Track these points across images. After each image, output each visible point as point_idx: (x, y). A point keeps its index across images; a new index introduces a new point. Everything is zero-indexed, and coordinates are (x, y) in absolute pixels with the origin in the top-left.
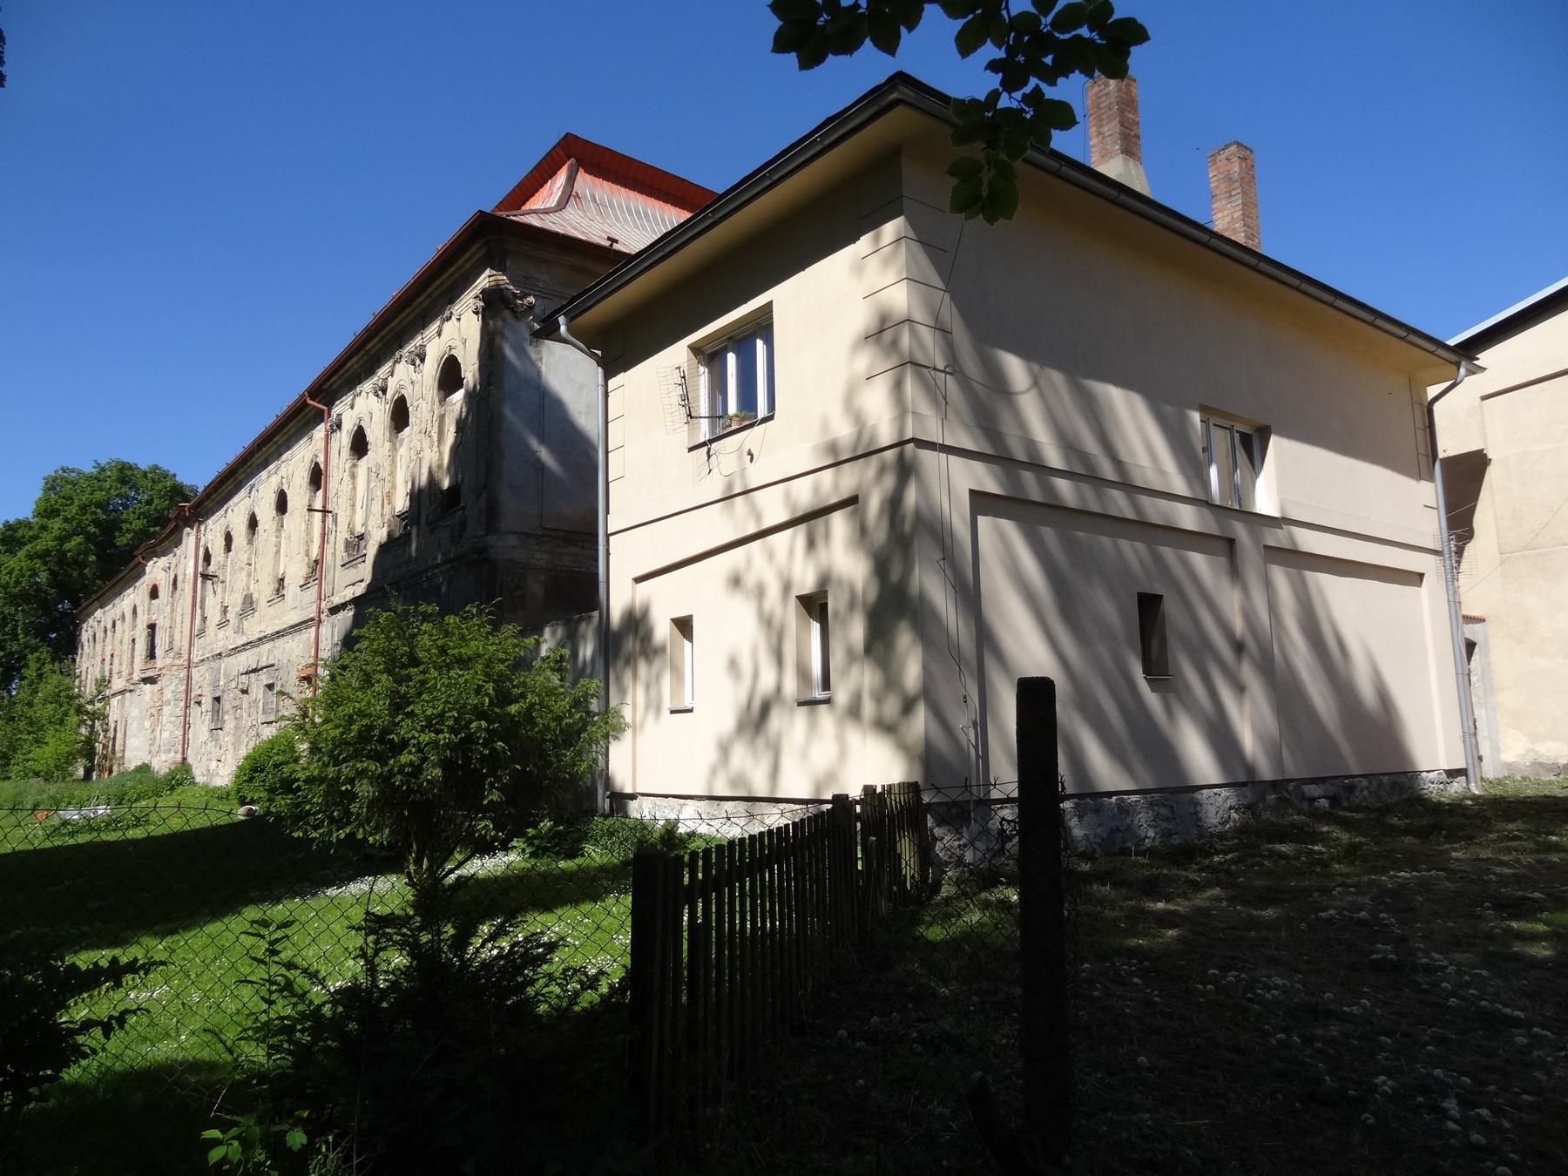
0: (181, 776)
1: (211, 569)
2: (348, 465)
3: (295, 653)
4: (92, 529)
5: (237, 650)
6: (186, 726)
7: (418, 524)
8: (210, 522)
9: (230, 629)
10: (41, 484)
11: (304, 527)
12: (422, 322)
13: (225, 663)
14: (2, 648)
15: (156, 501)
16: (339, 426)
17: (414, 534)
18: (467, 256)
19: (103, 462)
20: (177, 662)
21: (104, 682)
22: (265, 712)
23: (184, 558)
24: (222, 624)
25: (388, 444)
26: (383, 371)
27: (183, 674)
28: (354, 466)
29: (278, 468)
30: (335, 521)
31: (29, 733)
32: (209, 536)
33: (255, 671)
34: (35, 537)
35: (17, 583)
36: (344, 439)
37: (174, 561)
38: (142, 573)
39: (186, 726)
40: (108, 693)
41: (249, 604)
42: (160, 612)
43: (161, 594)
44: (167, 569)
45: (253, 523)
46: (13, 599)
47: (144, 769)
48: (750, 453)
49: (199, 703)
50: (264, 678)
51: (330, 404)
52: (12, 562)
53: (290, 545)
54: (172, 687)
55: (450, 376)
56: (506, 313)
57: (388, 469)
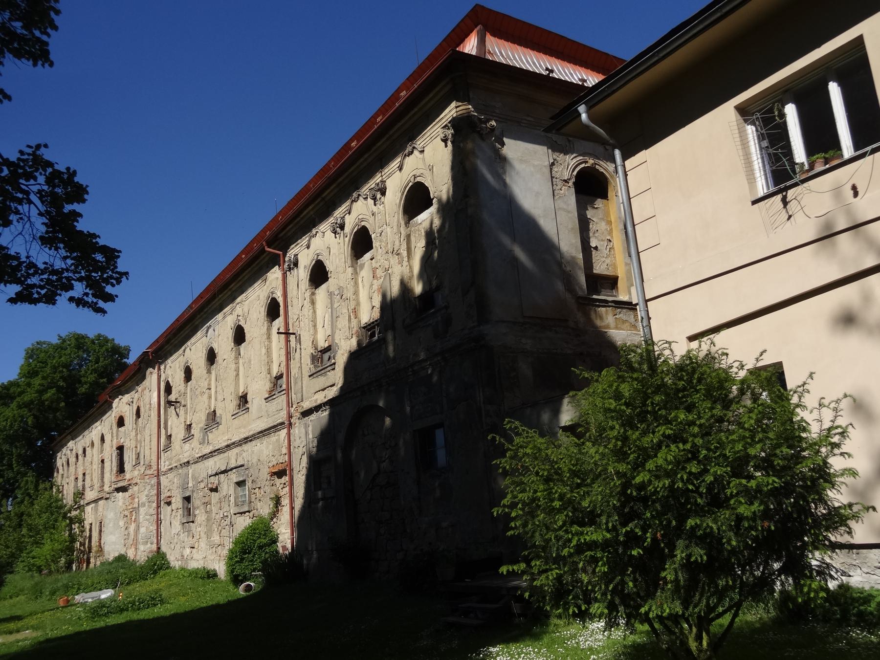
0: (158, 564)
1: (172, 398)
2: (308, 294)
3: (265, 454)
4: (61, 383)
5: (204, 457)
6: (159, 522)
7: (393, 329)
8: (169, 361)
9: (195, 442)
10: (23, 354)
11: (264, 351)
12: (381, 162)
13: (191, 470)
14: (1, 476)
16: (296, 264)
18: (431, 95)
19: (63, 335)
20: (148, 472)
21: (79, 494)
22: (236, 505)
24: (186, 440)
26: (339, 213)
27: (154, 481)
28: (313, 294)
29: (233, 309)
30: (299, 340)
31: (31, 537)
32: (169, 372)
33: (225, 472)
34: (22, 392)
35: (11, 426)
36: (302, 274)
39: (159, 522)
40: (82, 503)
41: (213, 418)
42: (127, 436)
43: (126, 422)
45: (211, 357)
46: (11, 439)
48: (854, 188)
50: (234, 477)
51: (285, 249)
52: (8, 412)
54: (146, 492)
55: (417, 198)
57: (352, 290)
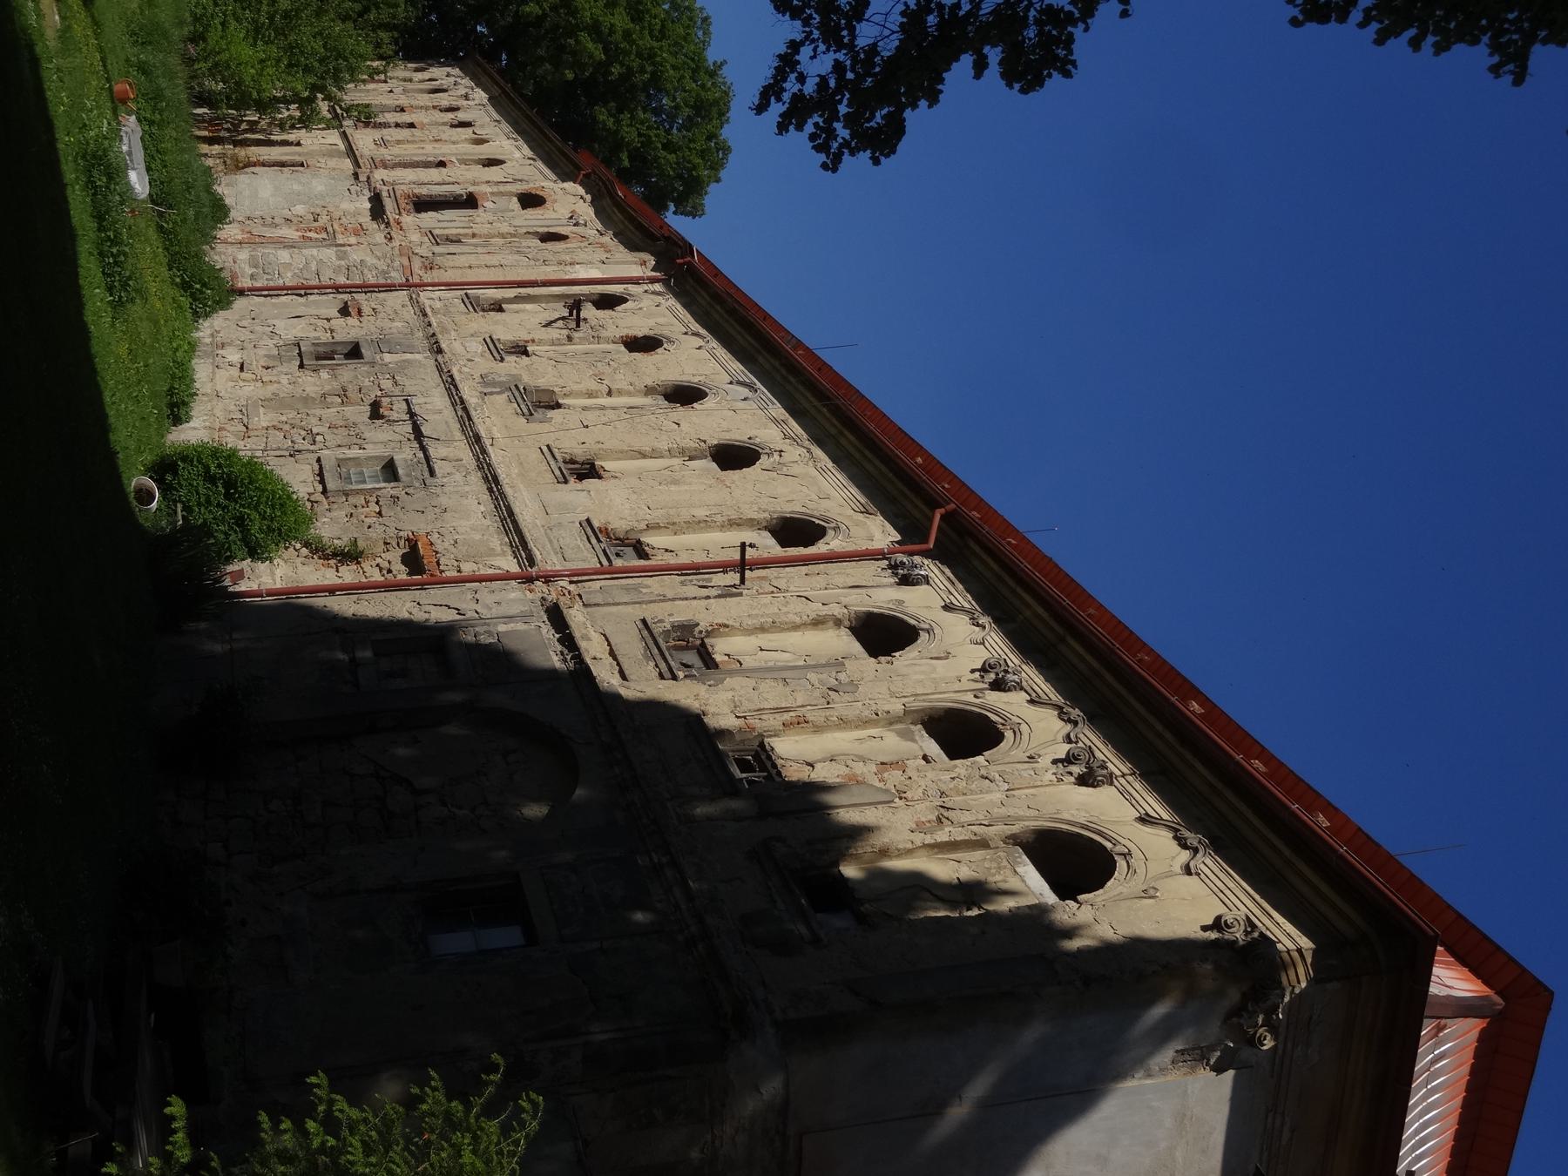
0: (207, 291)
1: (588, 311)
2: (837, 611)
3: (462, 525)
4: (616, 70)
5: (451, 386)
6: (302, 290)
8: (672, 302)
9: (486, 364)
11: (701, 513)
15: (672, 158)
16: (906, 581)
17: (736, 804)
18: (1324, 888)
21: (366, 117)
22: (340, 463)
23: (601, 258)
24: (492, 345)
25: (897, 707)
26: (1032, 676)
27: (397, 277)
28: (838, 623)
29: (794, 440)
30: (728, 593)
31: (271, 18)
32: (648, 302)
33: (418, 434)
36: (885, 596)
37: (591, 233)
39: (302, 290)
41: (543, 402)
49: (345, 312)
50: (406, 455)
51: (940, 555)
53: (662, 489)
54: (370, 260)
55: (1076, 861)
56: (1234, 996)
57: (851, 713)
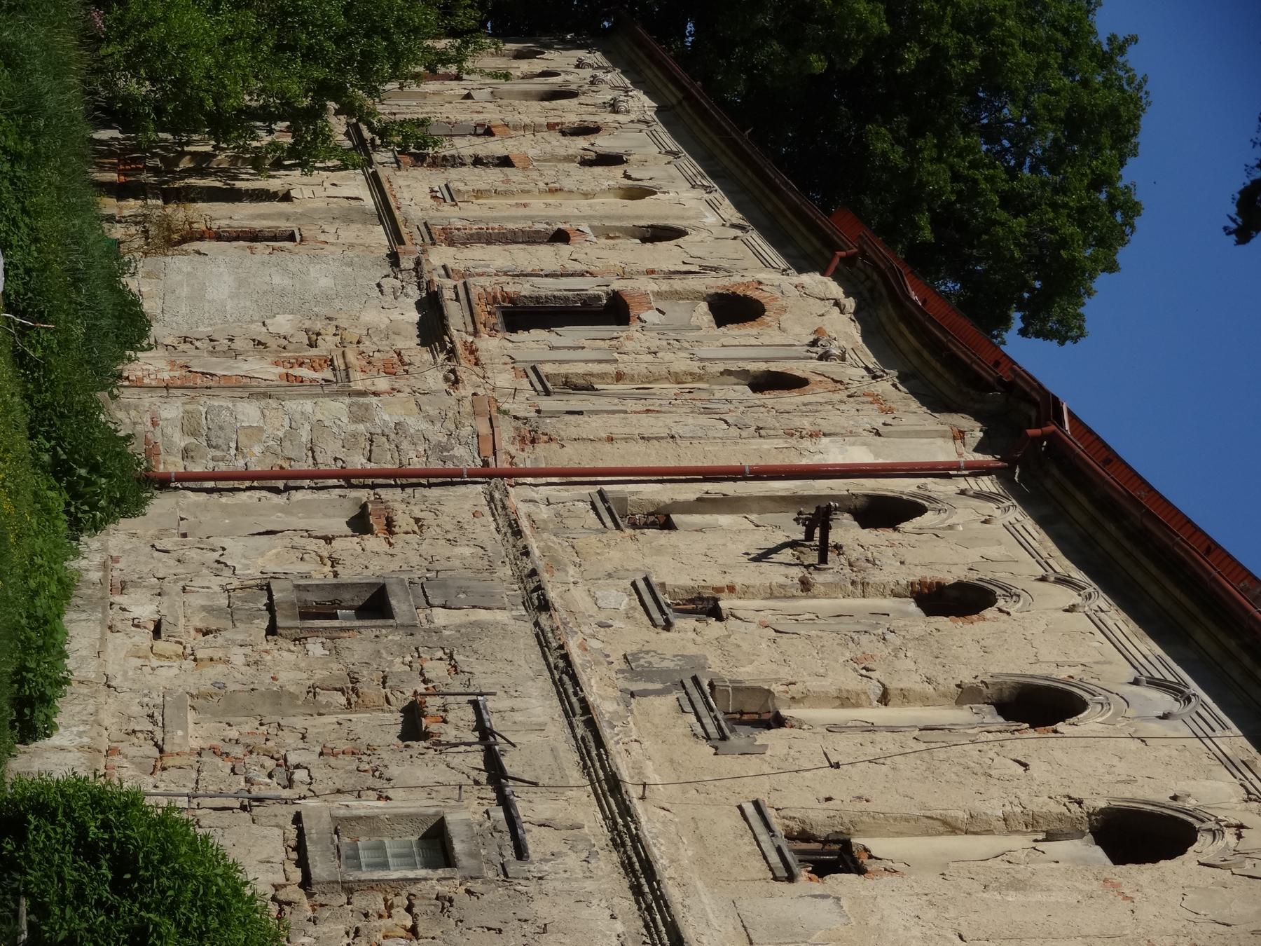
1: (845, 531)
4: (912, 55)
5: (565, 677)
6: (279, 481)
8: (1016, 514)
9: (635, 634)
13: (509, 619)
19: (1133, 58)
20: (506, 431)
21: (417, 144)
22: (340, 825)
23: (873, 425)
27: (465, 457)
32: (966, 514)
33: (495, 772)
38: (803, 260)
39: (279, 481)
41: (748, 714)
42: (673, 337)
44: (819, 346)
47: (131, 326)
49: (360, 524)
50: (469, 814)
54: (415, 423)
